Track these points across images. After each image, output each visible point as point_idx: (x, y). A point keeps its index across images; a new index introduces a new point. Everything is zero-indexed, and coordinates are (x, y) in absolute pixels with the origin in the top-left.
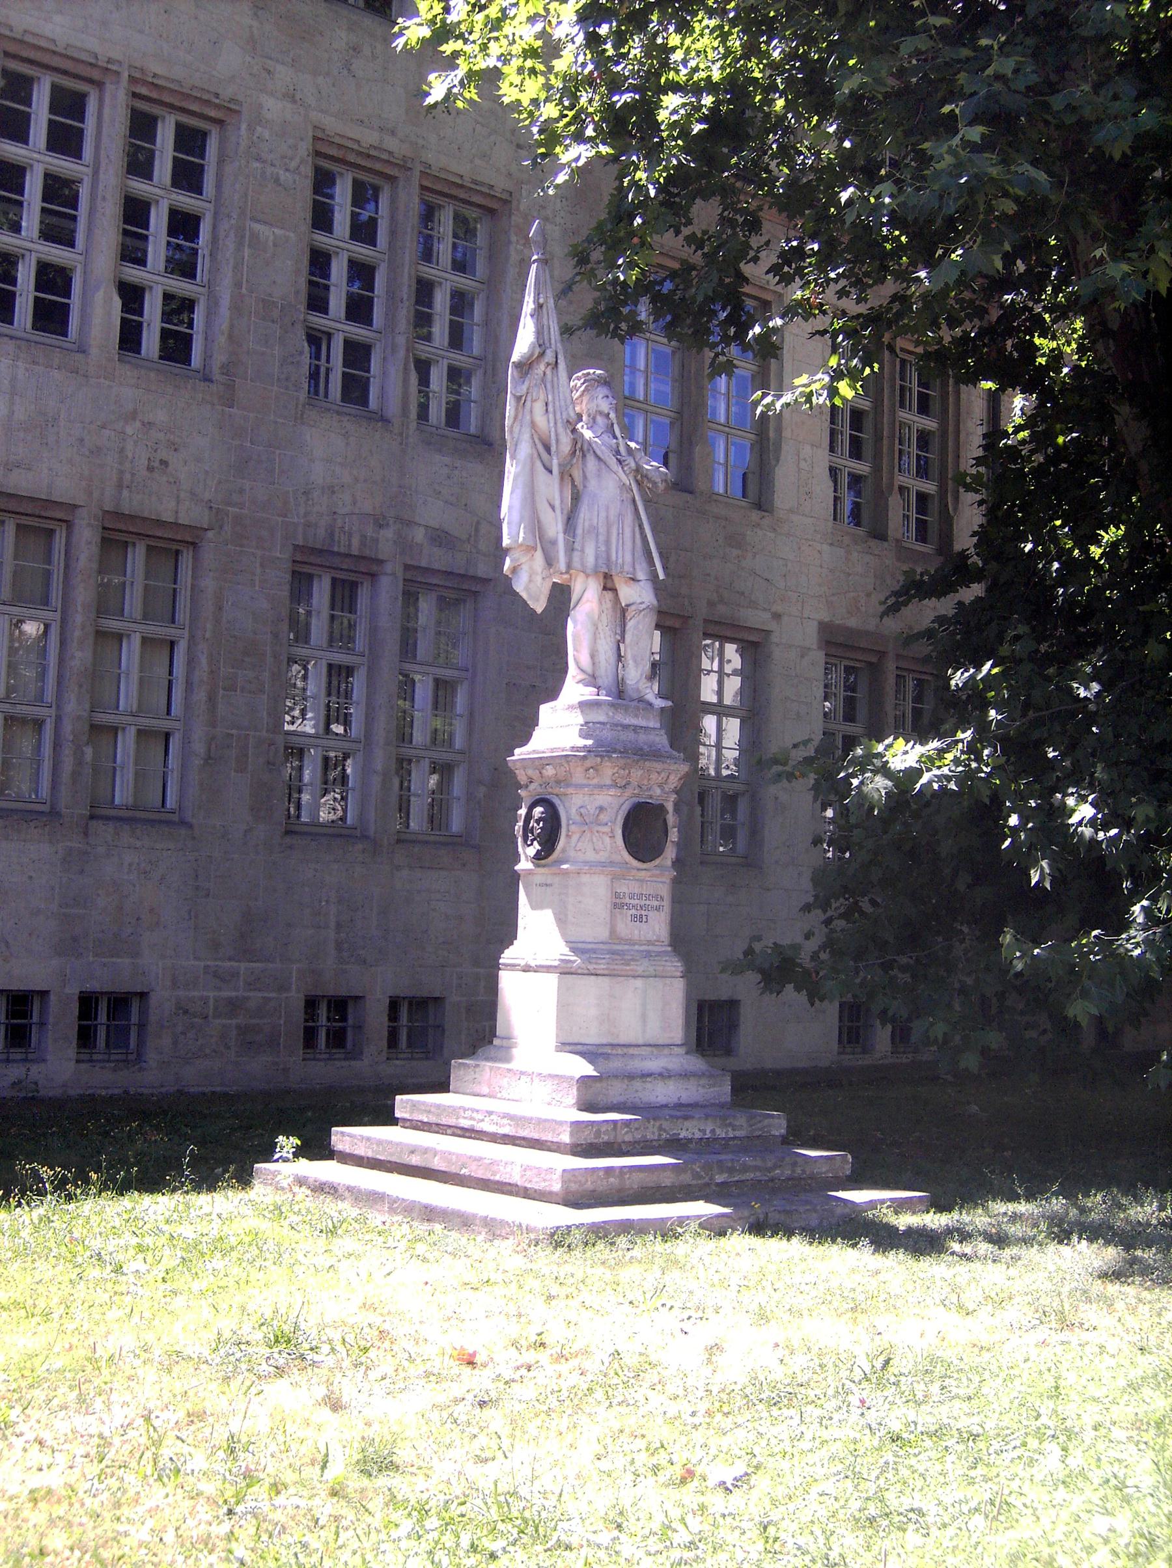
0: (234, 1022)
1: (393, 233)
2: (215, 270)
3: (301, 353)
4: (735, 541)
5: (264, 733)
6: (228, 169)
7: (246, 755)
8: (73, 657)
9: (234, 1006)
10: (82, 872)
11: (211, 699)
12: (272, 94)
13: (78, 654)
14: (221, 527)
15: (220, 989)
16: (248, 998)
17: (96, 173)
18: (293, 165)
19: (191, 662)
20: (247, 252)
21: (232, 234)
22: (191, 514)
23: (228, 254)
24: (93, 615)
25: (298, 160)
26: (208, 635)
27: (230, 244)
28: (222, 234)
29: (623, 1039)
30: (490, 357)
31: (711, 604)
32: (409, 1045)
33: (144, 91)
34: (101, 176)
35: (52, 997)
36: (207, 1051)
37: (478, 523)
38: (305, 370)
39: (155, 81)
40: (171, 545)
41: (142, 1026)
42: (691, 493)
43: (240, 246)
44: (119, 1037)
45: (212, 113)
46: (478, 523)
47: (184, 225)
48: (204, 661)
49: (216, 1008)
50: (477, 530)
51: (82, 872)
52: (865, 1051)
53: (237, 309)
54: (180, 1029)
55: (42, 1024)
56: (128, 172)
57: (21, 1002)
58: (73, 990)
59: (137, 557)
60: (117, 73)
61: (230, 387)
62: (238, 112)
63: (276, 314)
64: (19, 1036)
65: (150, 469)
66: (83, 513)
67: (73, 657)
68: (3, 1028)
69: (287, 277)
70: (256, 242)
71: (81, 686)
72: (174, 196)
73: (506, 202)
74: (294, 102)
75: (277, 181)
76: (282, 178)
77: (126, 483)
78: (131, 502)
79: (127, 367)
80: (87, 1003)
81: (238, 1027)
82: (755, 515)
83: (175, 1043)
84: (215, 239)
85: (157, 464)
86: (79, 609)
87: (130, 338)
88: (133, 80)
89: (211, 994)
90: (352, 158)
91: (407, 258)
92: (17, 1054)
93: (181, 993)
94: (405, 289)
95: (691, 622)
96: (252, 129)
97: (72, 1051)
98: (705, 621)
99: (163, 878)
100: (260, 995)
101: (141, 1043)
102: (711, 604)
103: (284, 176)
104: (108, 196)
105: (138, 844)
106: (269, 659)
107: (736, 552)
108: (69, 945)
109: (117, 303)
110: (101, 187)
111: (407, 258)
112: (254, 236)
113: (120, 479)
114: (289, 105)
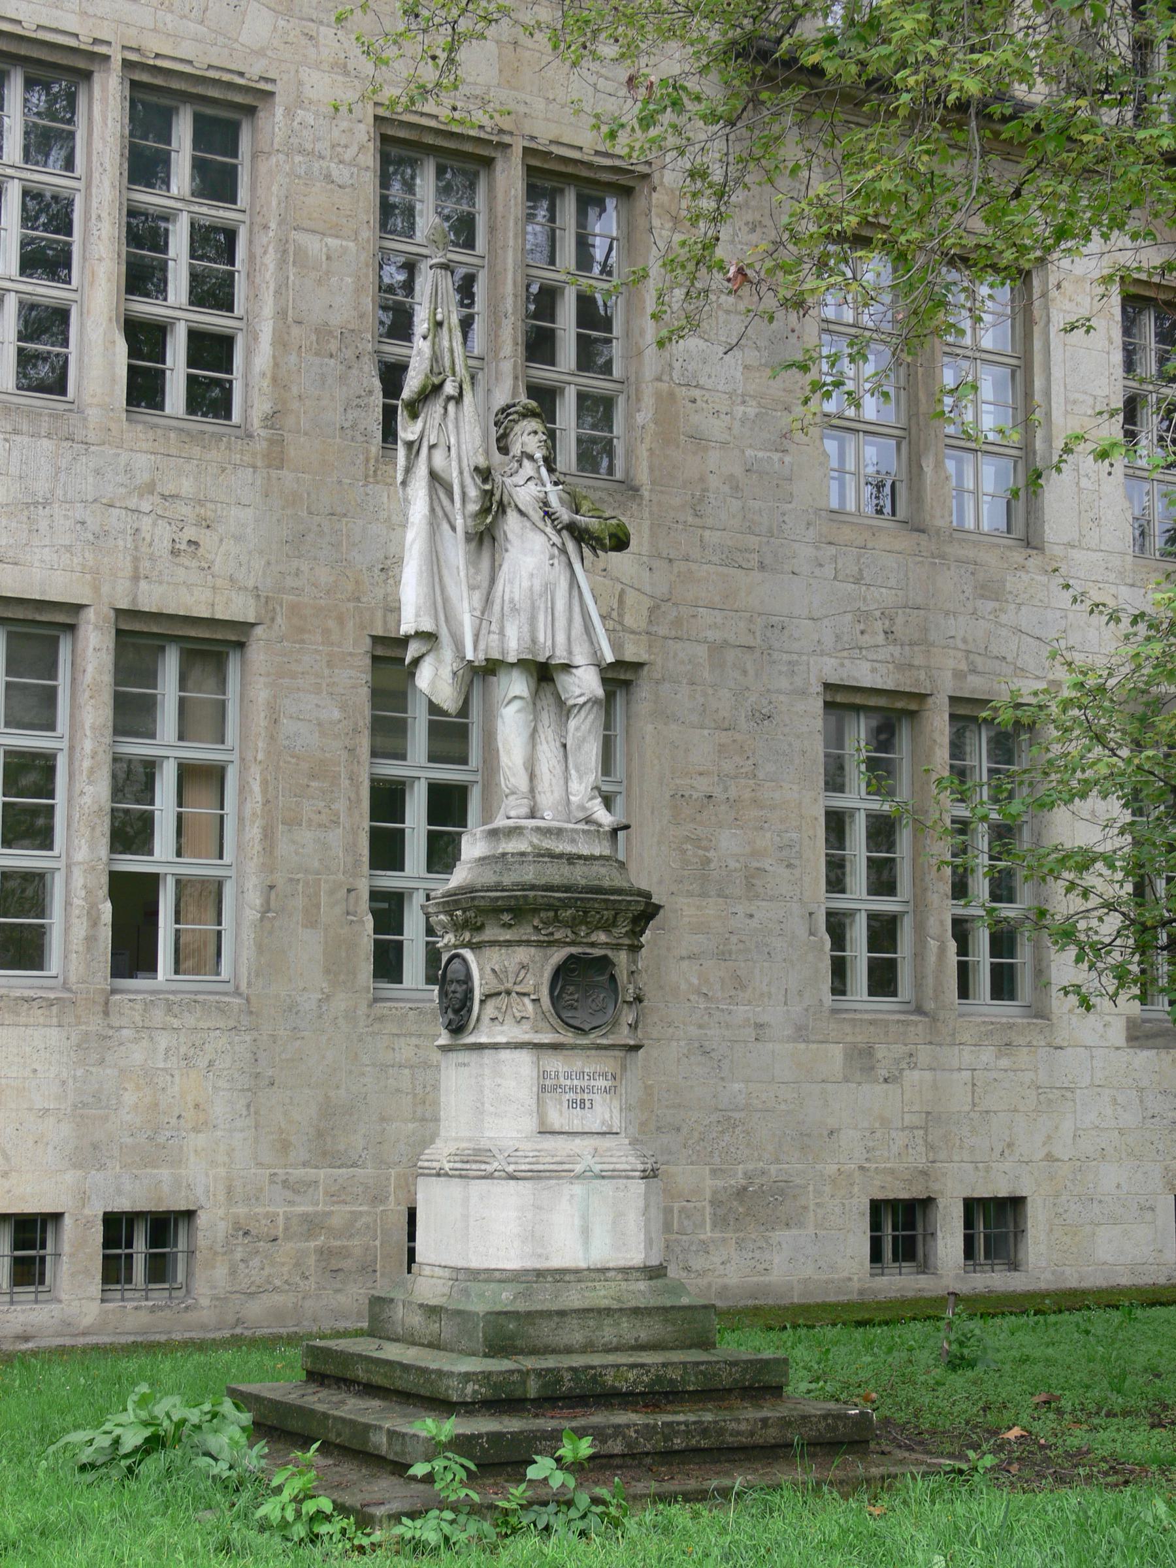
0: (312, 1244)
1: (492, 229)
2: (254, 296)
3: (371, 392)
4: (991, 590)
5: (341, 876)
6: (263, 167)
7: (318, 906)
8: (82, 793)
9: (312, 1225)
10: (102, 1062)
11: (268, 835)
12: (318, 65)
13: (89, 789)
14: (273, 619)
15: (291, 1203)
16: (329, 1214)
17: (88, 187)
18: (348, 155)
19: (243, 789)
20: (292, 271)
21: (271, 250)
22: (235, 607)
23: (268, 275)
24: (108, 739)
25: (354, 149)
26: (260, 757)
27: (270, 260)
28: (259, 251)
29: (556, 1263)
30: (632, 379)
31: (959, 675)
32: (987, 1257)
33: (145, 78)
34: (94, 190)
35: (67, 1221)
36: (278, 1283)
37: (622, 594)
38: (378, 414)
39: (160, 63)
40: (211, 648)
41: (191, 1253)
42: (923, 531)
43: (282, 263)
44: (159, 1270)
45: (239, 98)
46: (622, 594)
47: (216, 243)
48: (256, 788)
49: (286, 1229)
50: (621, 601)
51: (102, 1062)
52: (1014, 1266)
53: (281, 342)
54: (238, 1256)
55: (58, 1255)
56: (132, 180)
57: (31, 1231)
58: (96, 1210)
59: (170, 665)
60: (107, 58)
61: (277, 443)
62: (271, 94)
63: (333, 346)
64: (28, 1272)
65: (175, 553)
66: (90, 615)
67: (82, 793)
68: (7, 1262)
69: (348, 301)
70: (301, 258)
71: (93, 829)
72: (196, 209)
73: (645, 177)
74: (346, 73)
75: (329, 179)
76: (335, 174)
77: (142, 572)
78: (151, 599)
79: (140, 427)
80: (117, 1227)
81: (320, 1251)
82: (1018, 556)
83: (233, 1272)
84: (252, 257)
85: (183, 546)
86: (88, 733)
87: (144, 390)
88: (127, 64)
89: (281, 1211)
90: (429, 140)
91: (510, 261)
92: (26, 1293)
93: (241, 1210)
94: (510, 301)
95: (930, 700)
96: (289, 113)
97: (95, 1285)
98: (953, 700)
99: (211, 1064)
100: (348, 1208)
101: (189, 1274)
102: (959, 675)
103: (337, 171)
104: (104, 215)
105: (176, 1023)
106: (345, 783)
107: (991, 605)
108: (87, 1155)
109: (122, 347)
110: (94, 205)
111: (510, 261)
112: (300, 251)
113: (136, 569)
114: (340, 78)
